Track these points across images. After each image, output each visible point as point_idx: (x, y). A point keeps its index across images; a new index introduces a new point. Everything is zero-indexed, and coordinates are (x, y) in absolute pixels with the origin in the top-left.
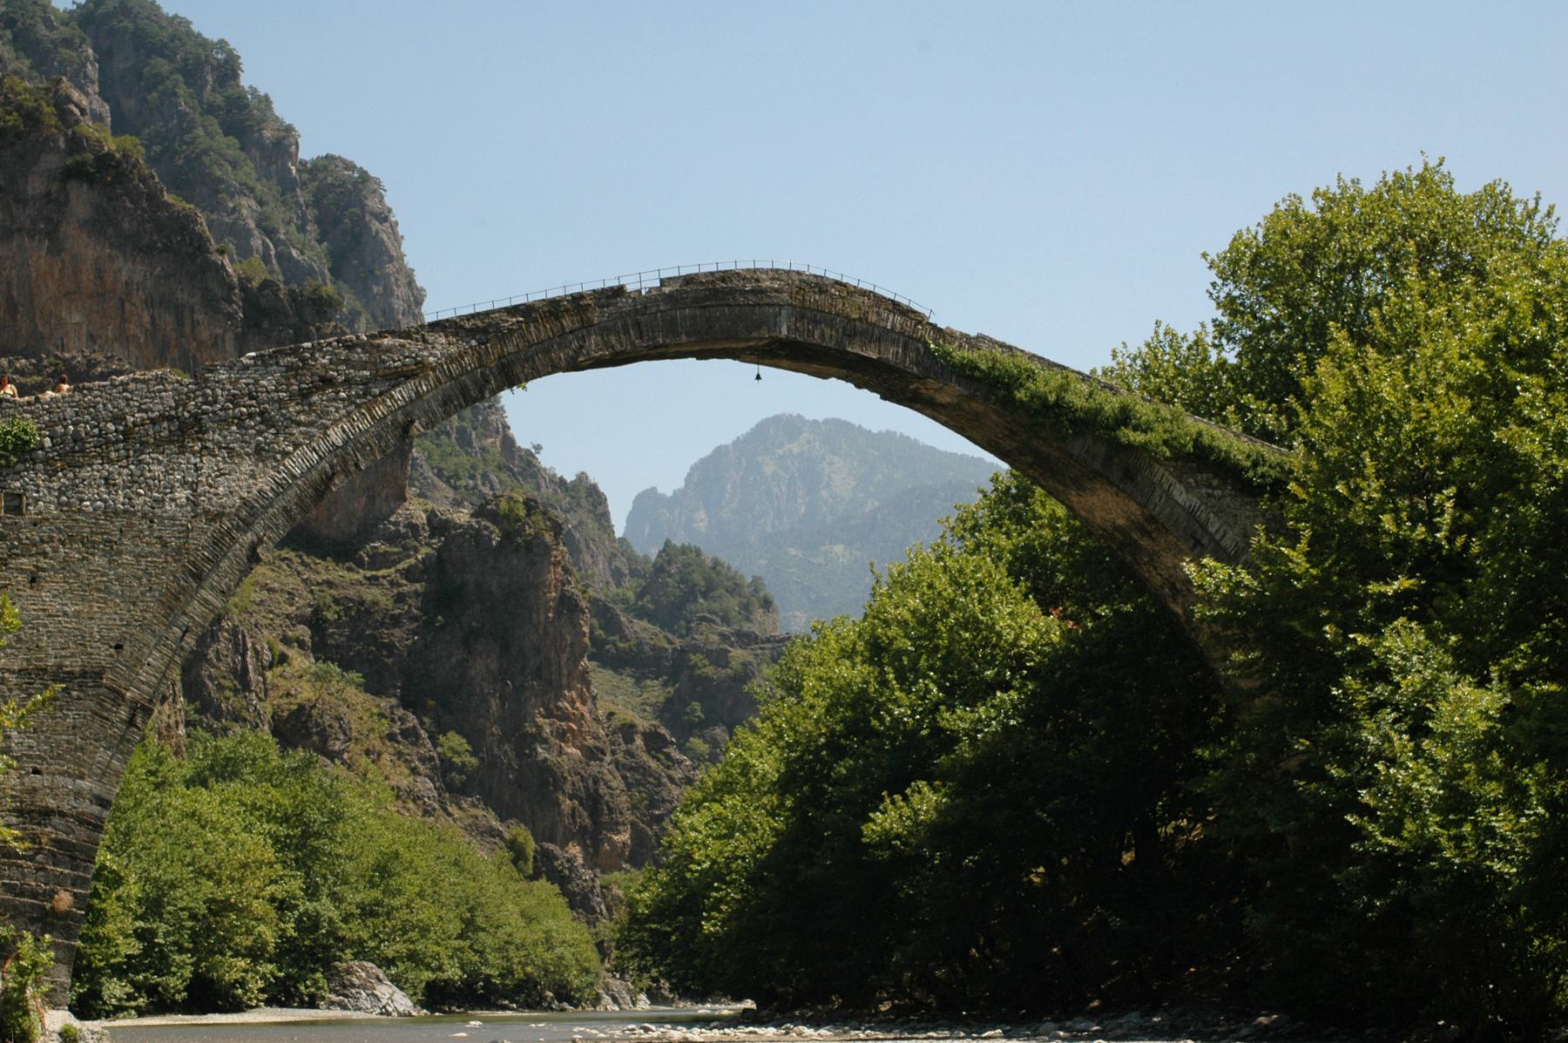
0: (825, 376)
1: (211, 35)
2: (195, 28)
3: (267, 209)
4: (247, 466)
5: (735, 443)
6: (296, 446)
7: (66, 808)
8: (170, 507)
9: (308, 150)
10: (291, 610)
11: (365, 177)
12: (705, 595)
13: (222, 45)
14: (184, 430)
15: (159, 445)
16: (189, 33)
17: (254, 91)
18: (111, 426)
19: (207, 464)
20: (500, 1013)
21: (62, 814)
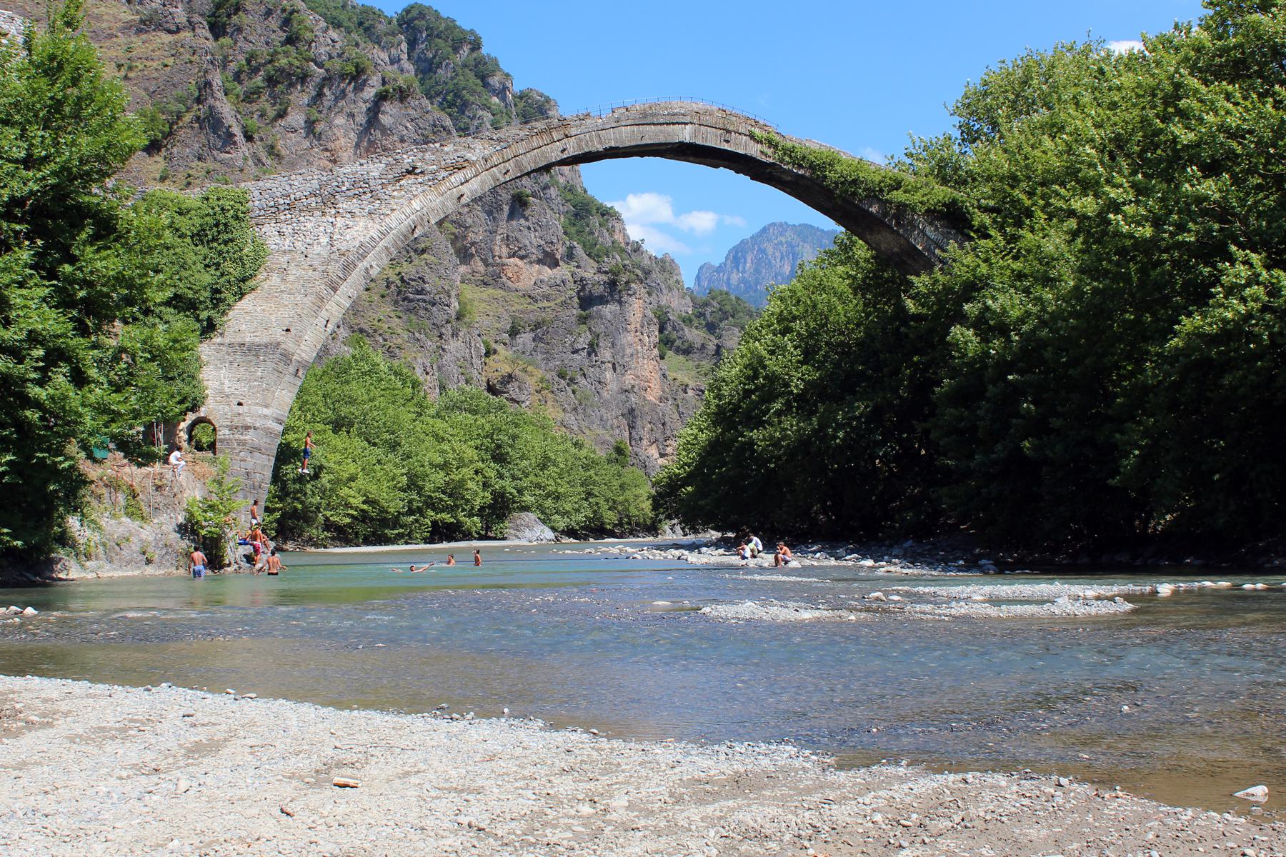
0: (717, 167)
1: (467, 27)
2: (458, 23)
3: (498, 117)
4: (362, 223)
5: (752, 237)
6: (393, 210)
7: (257, 425)
8: (317, 249)
9: (517, 86)
10: (498, 325)
11: (548, 100)
12: (733, 316)
13: (472, 32)
14: (327, 200)
15: (310, 210)
16: (456, 27)
17: (489, 55)
18: (281, 201)
19: (340, 222)
20: (322, 550)
21: (255, 428)
